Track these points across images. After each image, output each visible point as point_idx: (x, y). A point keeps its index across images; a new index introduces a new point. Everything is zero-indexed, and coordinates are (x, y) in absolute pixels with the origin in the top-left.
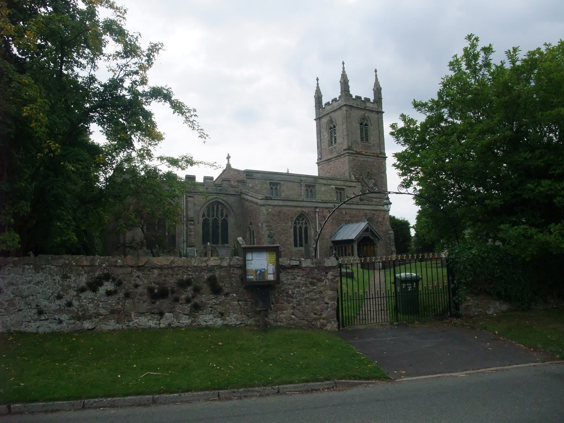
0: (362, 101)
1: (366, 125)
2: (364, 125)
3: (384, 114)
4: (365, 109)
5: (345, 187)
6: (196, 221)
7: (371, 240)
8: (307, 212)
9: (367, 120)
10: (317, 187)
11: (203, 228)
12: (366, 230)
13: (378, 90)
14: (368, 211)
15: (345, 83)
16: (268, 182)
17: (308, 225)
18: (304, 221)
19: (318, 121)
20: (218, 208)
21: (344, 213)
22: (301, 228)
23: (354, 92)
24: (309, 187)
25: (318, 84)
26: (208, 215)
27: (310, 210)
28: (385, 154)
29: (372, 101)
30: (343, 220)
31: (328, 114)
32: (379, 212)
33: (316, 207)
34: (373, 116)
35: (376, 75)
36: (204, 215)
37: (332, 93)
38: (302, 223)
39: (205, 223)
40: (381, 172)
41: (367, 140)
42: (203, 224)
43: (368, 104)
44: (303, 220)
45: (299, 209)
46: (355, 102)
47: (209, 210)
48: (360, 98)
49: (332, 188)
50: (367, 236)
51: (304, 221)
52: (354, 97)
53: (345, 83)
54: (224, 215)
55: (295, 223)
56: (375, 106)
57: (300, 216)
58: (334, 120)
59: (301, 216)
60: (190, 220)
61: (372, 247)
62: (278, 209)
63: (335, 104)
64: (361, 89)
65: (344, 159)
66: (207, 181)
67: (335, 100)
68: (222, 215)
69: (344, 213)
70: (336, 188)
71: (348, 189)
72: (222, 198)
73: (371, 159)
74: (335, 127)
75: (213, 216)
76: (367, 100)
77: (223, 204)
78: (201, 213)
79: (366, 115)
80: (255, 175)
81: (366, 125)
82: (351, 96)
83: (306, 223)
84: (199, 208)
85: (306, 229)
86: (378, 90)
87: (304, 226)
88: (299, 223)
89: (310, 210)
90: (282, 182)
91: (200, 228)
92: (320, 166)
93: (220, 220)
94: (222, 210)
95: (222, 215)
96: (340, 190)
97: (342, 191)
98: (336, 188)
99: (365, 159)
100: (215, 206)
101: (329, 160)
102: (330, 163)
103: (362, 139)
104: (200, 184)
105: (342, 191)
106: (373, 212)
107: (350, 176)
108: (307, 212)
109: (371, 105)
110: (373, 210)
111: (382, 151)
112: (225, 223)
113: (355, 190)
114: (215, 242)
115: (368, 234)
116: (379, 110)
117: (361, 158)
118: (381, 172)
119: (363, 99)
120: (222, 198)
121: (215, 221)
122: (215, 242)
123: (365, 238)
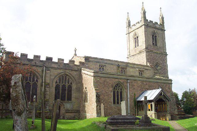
0: (153, 23)
3: (165, 32)
6: (51, 85)
7: (163, 101)
10: (128, 69)
11: (56, 90)
12: (160, 94)
16: (98, 64)
20: (66, 78)
22: (118, 92)
24: (123, 69)
26: (59, 82)
31: (134, 30)
34: (160, 32)
36: (56, 82)
39: (57, 88)
41: (156, 45)
42: (56, 87)
44: (119, 87)
45: (117, 80)
47: (60, 80)
48: (152, 22)
49: (137, 70)
52: (149, 21)
54: (70, 82)
55: (114, 89)
57: (117, 84)
59: (118, 85)
60: (47, 85)
62: (103, 79)
64: (154, 17)
66: (60, 61)
68: (68, 83)
69: (145, 84)
70: (139, 70)
71: (146, 71)
72: (69, 72)
74: (138, 37)
75: (63, 83)
76: (156, 23)
77: (69, 76)
78: (55, 81)
80: (90, 59)
82: (147, 20)
83: (121, 89)
84: (54, 77)
85: (121, 93)
87: (119, 91)
88: (117, 89)
90: (106, 65)
91: (53, 90)
93: (31, 83)
94: (68, 80)
95: (33, 80)
96: (141, 72)
98: (139, 70)
100: (63, 78)
104: (55, 63)
106: (162, 84)
108: (122, 82)
112: (70, 87)
114: (63, 99)
115: (162, 97)
116: (163, 29)
119: (154, 23)
120: (68, 72)
121: (64, 86)
122: (63, 99)
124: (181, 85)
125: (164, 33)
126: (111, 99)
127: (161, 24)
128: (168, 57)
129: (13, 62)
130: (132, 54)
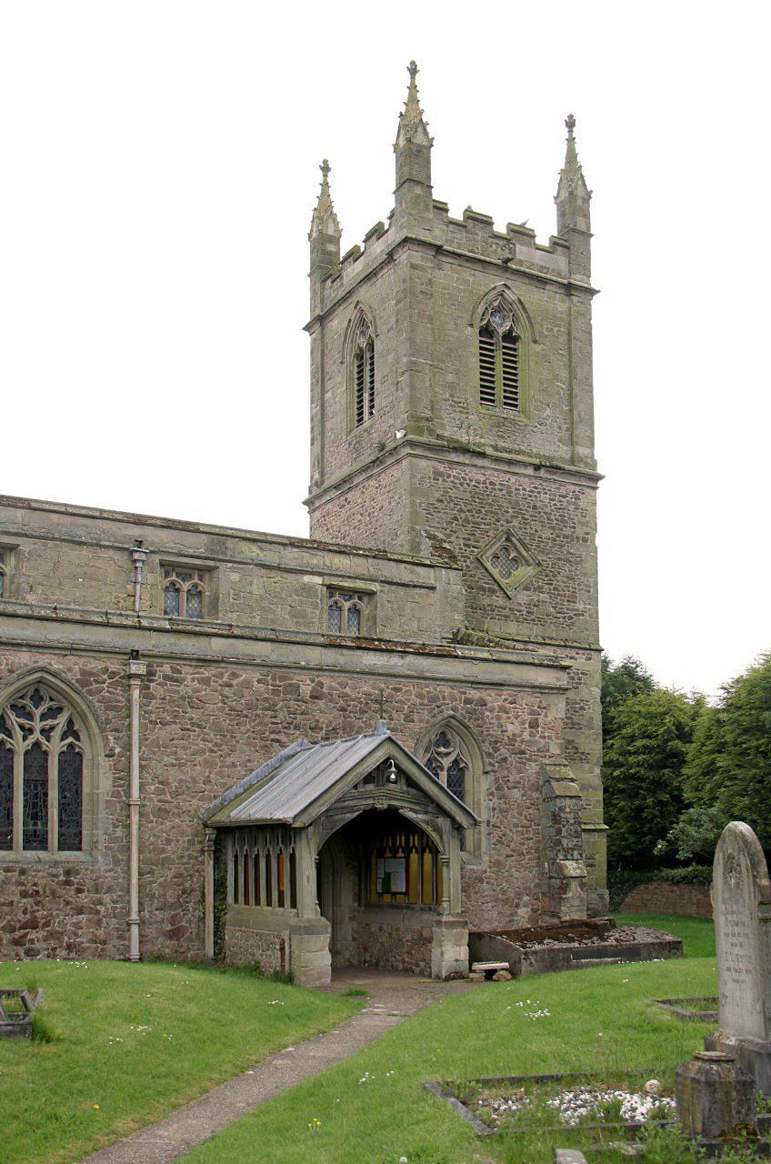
1: (510, 337)
2: (499, 345)
3: (433, 190)
4: (504, 267)
5: (375, 587)
8: (73, 677)
9: (515, 319)
10: (229, 577)
13: (574, 201)
14: (446, 689)
15: (414, 154)
17: (84, 745)
18: (61, 720)
19: (317, 327)
21: (306, 689)
23: (454, 187)
25: (325, 185)
27: (95, 665)
28: (594, 466)
29: (543, 240)
30: (286, 719)
32: (506, 693)
33: (135, 654)
35: (571, 140)
37: (367, 204)
38: (46, 732)
40: (571, 539)
43: (521, 251)
44: (52, 713)
46: (460, 236)
48: (486, 222)
49: (308, 590)
50: (382, 805)
51: (61, 720)
53: (414, 154)
56: (560, 261)
58: (369, 317)
61: (428, 857)
63: (379, 248)
64: (495, 183)
65: (395, 472)
67: (377, 232)
69: (306, 689)
70: (331, 588)
73: (523, 482)
76: (521, 233)
79: (510, 296)
81: (510, 337)
82: (442, 208)
83: (70, 731)
85: (72, 763)
86: (574, 201)
87: (55, 747)
88: (28, 731)
89: (95, 665)
90: (25, 545)
92: (317, 514)
97: (362, 605)
99: (499, 478)
101: (345, 484)
102: (350, 496)
103: (487, 394)
105: (362, 605)
106: (474, 694)
107: (416, 547)
108: (73, 677)
109: (539, 258)
110: (476, 684)
111: (582, 451)
113: (433, 609)
116: (577, 280)
117: (478, 473)
118: (571, 539)
123: (370, 815)
124: (684, 609)
125: (586, 315)
126: (497, 570)
127: (555, 243)
128: (604, 492)
129: (3, 496)
130: (335, 476)
